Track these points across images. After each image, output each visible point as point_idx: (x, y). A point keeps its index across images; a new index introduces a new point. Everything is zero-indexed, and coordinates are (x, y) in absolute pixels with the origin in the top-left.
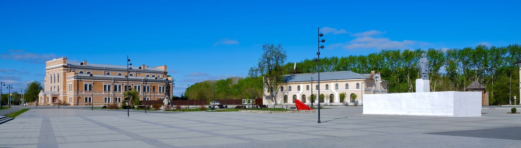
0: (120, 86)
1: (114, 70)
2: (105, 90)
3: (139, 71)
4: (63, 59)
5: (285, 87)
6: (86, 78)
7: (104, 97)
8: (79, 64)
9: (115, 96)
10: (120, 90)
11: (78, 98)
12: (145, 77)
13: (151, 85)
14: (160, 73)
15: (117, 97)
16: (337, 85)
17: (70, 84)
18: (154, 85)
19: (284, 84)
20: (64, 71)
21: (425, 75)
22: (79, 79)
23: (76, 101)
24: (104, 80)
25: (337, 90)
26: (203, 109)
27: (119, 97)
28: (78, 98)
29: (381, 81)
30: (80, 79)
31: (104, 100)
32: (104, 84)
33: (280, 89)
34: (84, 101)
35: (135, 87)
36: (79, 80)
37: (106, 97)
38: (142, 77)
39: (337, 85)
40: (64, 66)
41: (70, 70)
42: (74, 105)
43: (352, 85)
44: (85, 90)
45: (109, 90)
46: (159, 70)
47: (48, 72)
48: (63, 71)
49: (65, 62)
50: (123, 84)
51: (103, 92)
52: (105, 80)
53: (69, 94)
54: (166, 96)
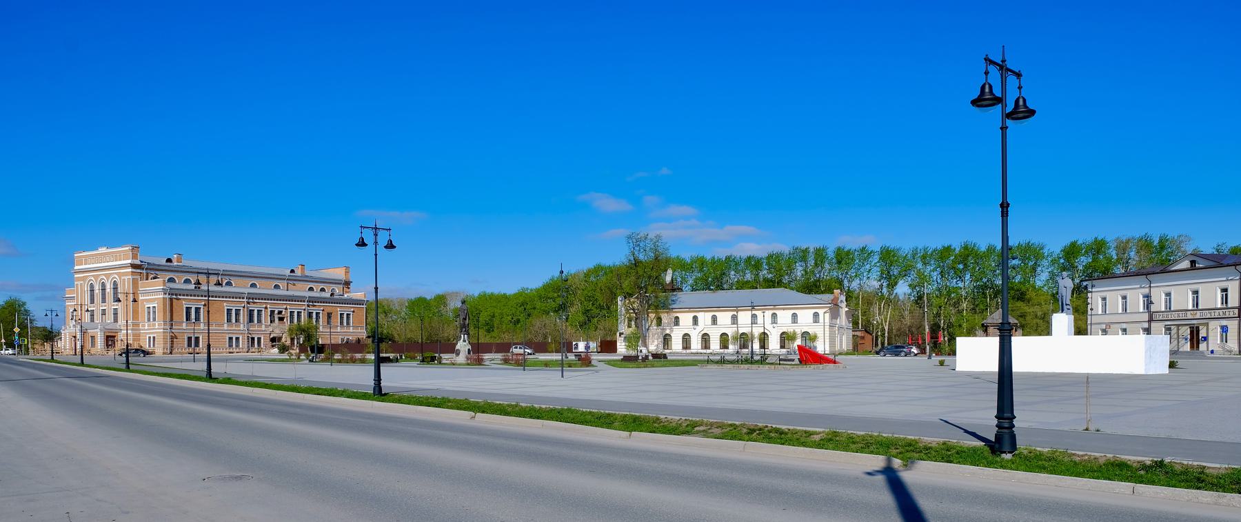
0: (259, 312)
1: (241, 276)
2: (229, 320)
3: (167, 268)
4: (131, 248)
5: (665, 318)
6: (189, 293)
7: (148, 336)
8: (163, 262)
9: (250, 334)
10: (259, 321)
11: (173, 338)
12: (271, 289)
13: (323, 310)
14: (336, 283)
15: (253, 336)
16: (774, 316)
17: (151, 306)
18: (329, 310)
19: (664, 313)
20: (135, 277)
21: (1068, 307)
22: (172, 294)
23: (169, 346)
24: (226, 297)
25: (775, 325)
26: (353, 361)
27: (237, 336)
28: (172, 338)
29: (847, 309)
30: (176, 295)
31: (227, 342)
32: (226, 306)
33: (655, 321)
34: (186, 345)
35: (292, 313)
36: (174, 297)
37: (230, 336)
38: (301, 290)
39: (774, 316)
40: (133, 266)
41: (147, 274)
42: (164, 353)
43: (805, 316)
44: (187, 320)
45: (237, 320)
46: (328, 277)
47: (84, 279)
48: (130, 277)
49: (134, 257)
50: (266, 308)
51: (226, 325)
52: (230, 297)
53: (147, 330)
54: (462, 336)
